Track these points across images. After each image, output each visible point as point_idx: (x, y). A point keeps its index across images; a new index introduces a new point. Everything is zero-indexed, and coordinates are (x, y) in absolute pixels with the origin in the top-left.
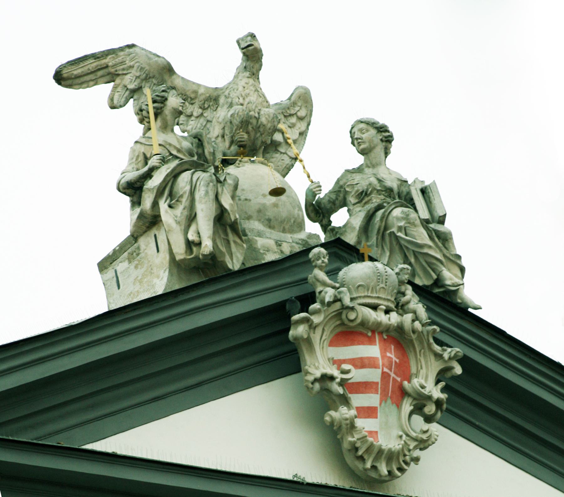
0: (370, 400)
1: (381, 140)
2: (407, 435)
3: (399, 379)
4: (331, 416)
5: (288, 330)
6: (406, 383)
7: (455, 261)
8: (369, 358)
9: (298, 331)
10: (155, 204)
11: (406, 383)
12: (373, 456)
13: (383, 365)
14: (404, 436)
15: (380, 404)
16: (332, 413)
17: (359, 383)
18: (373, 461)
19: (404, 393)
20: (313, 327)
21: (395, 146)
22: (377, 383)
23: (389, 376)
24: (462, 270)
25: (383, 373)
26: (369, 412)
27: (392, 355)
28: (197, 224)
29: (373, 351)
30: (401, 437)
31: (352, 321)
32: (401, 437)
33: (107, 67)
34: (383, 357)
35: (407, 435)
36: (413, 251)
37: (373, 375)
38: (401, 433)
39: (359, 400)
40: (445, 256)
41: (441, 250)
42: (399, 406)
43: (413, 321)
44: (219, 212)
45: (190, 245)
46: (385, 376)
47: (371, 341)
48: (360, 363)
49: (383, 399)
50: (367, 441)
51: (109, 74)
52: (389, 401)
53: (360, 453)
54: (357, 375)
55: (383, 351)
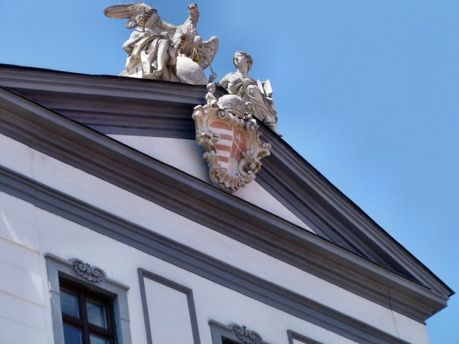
0: (227, 154)
1: (247, 62)
2: (241, 174)
3: (240, 150)
4: (206, 155)
5: (192, 112)
6: (243, 153)
7: (274, 113)
8: (228, 136)
9: (197, 113)
10: (139, 52)
11: (243, 153)
12: (224, 177)
13: (234, 140)
14: (239, 174)
15: (230, 157)
16: (207, 153)
17: (222, 146)
18: (223, 180)
19: (242, 157)
20: (204, 114)
21: (253, 66)
22: (230, 148)
23: (236, 147)
24: (276, 119)
25: (233, 143)
26: (225, 160)
27: (239, 137)
28: (157, 61)
29: (231, 133)
30: (238, 174)
31: (223, 116)
32: (238, 174)
33: (128, 11)
34: (235, 136)
35: (241, 174)
36: (255, 104)
37: (229, 143)
38: (238, 172)
39: (221, 153)
40: (269, 110)
41: (268, 108)
42: (239, 162)
43: (251, 125)
44: (168, 58)
45: (152, 69)
46: (234, 146)
47: (230, 129)
48: (224, 137)
49: (232, 155)
50: (222, 171)
51: (128, 14)
52: (234, 157)
53: (217, 175)
54: (222, 142)
55: (235, 135)
